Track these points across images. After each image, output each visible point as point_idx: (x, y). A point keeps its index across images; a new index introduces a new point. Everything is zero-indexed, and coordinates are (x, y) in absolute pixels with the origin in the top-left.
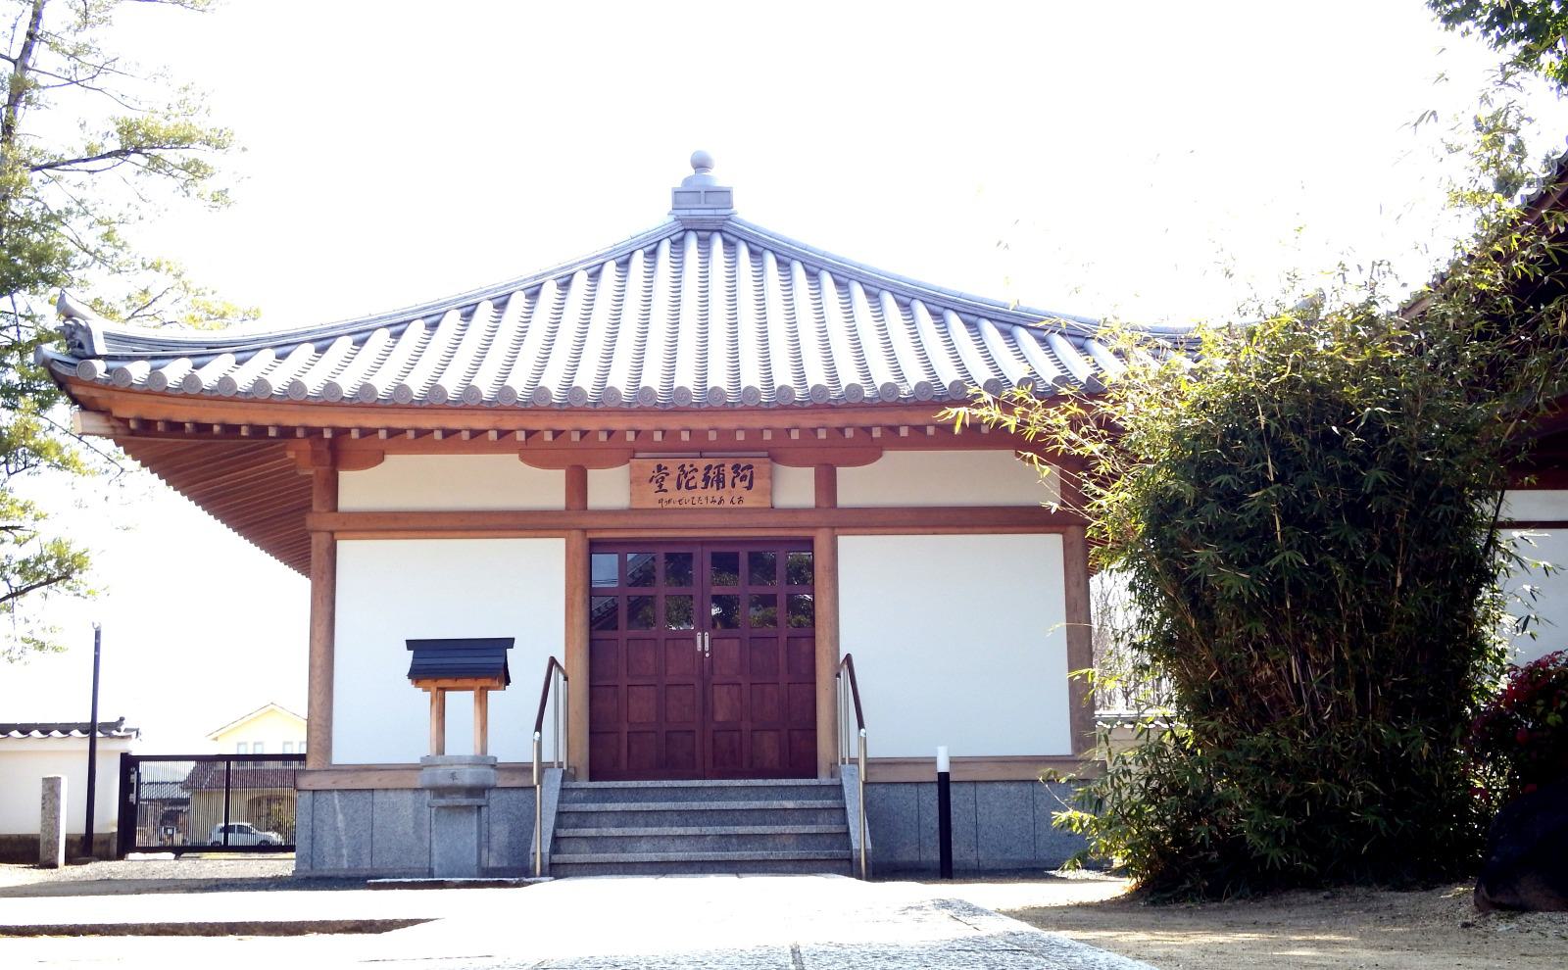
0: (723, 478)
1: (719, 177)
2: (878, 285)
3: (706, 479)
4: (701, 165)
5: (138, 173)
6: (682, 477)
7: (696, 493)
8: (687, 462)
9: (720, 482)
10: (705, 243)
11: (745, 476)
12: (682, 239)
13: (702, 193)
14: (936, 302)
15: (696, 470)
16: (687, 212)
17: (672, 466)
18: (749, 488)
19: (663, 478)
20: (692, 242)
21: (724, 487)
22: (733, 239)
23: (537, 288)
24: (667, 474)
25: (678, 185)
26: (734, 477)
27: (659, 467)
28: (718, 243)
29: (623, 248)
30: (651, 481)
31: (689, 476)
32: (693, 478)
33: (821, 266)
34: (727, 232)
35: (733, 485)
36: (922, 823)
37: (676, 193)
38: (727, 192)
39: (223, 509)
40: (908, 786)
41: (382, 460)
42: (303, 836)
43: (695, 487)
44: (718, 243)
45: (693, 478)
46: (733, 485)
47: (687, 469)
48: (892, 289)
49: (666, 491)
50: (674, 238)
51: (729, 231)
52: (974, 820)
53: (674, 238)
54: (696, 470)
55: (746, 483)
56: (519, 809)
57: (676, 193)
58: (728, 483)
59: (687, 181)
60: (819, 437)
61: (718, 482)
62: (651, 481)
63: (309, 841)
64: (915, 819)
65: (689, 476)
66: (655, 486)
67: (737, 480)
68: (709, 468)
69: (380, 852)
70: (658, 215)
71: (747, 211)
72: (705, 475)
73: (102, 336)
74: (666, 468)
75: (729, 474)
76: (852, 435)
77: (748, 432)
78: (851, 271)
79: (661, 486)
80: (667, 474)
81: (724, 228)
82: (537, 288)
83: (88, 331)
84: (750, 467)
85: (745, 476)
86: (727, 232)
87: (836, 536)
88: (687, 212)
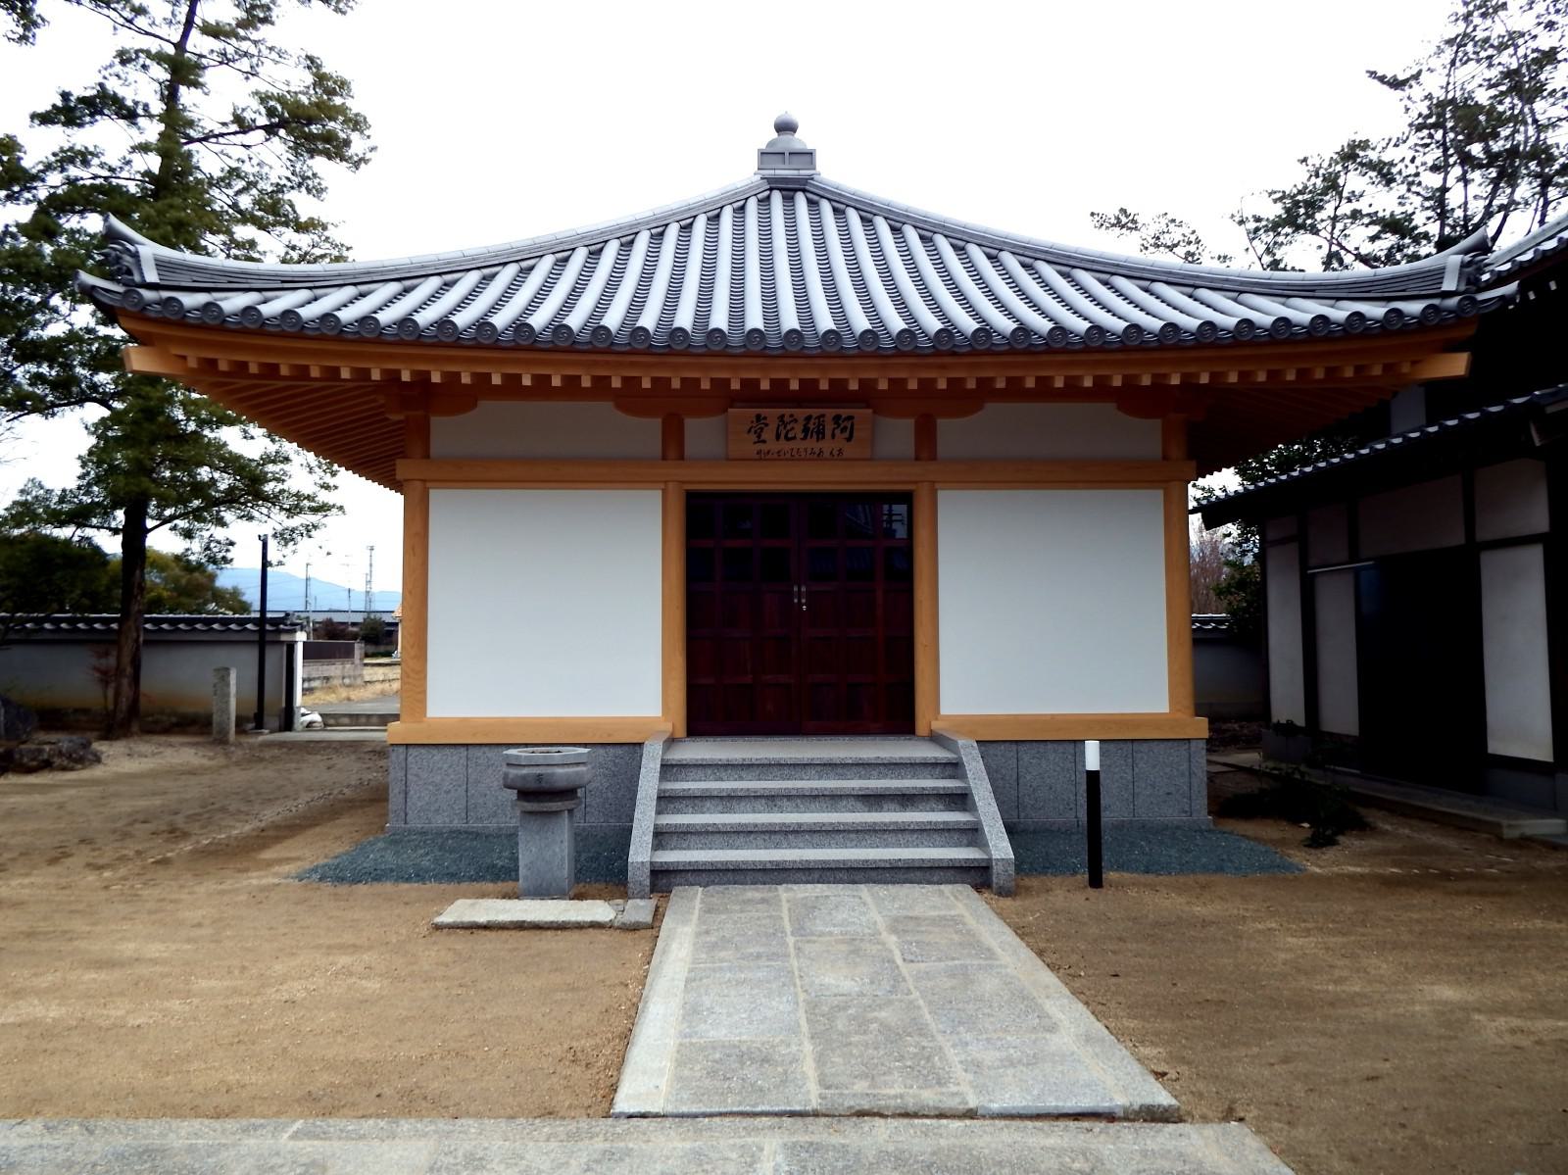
0: (824, 429)
1: (804, 138)
2: (964, 238)
3: (806, 430)
4: (785, 127)
5: (348, 249)
6: (781, 428)
7: (792, 444)
8: (787, 411)
9: (820, 434)
10: (789, 200)
11: (845, 428)
12: (768, 198)
13: (787, 154)
14: (1026, 253)
15: (796, 421)
16: (772, 172)
17: (772, 413)
18: (849, 439)
19: (762, 429)
20: (777, 198)
21: (823, 437)
22: (815, 198)
23: (632, 237)
24: (767, 425)
25: (763, 147)
26: (834, 429)
27: (758, 417)
28: (801, 200)
29: (715, 202)
30: (749, 431)
31: (789, 427)
32: (793, 428)
33: (903, 220)
34: (809, 191)
35: (833, 436)
36: (1021, 781)
37: (763, 154)
38: (811, 153)
39: (330, 449)
40: (1007, 744)
41: (474, 406)
42: (396, 791)
43: (794, 438)
44: (801, 200)
45: (793, 428)
46: (833, 436)
47: (787, 419)
48: (979, 242)
49: (764, 442)
50: (760, 196)
51: (812, 189)
52: (1073, 778)
53: (760, 196)
54: (796, 421)
55: (847, 434)
56: (615, 765)
57: (763, 154)
58: (828, 433)
59: (771, 144)
60: (703, 387)
61: (818, 433)
62: (749, 431)
63: (402, 795)
64: (1015, 777)
65: (789, 427)
66: (754, 437)
67: (838, 432)
68: (808, 418)
69: (475, 807)
70: (744, 172)
71: (829, 171)
72: (805, 426)
73: (153, 263)
74: (765, 418)
75: (829, 427)
76: (974, 387)
77: (744, 382)
78: (935, 225)
79: (759, 437)
80: (767, 425)
81: (807, 187)
82: (632, 237)
83: (136, 256)
84: (850, 418)
85: (845, 428)
86: (809, 191)
87: (936, 490)
88: (772, 172)
